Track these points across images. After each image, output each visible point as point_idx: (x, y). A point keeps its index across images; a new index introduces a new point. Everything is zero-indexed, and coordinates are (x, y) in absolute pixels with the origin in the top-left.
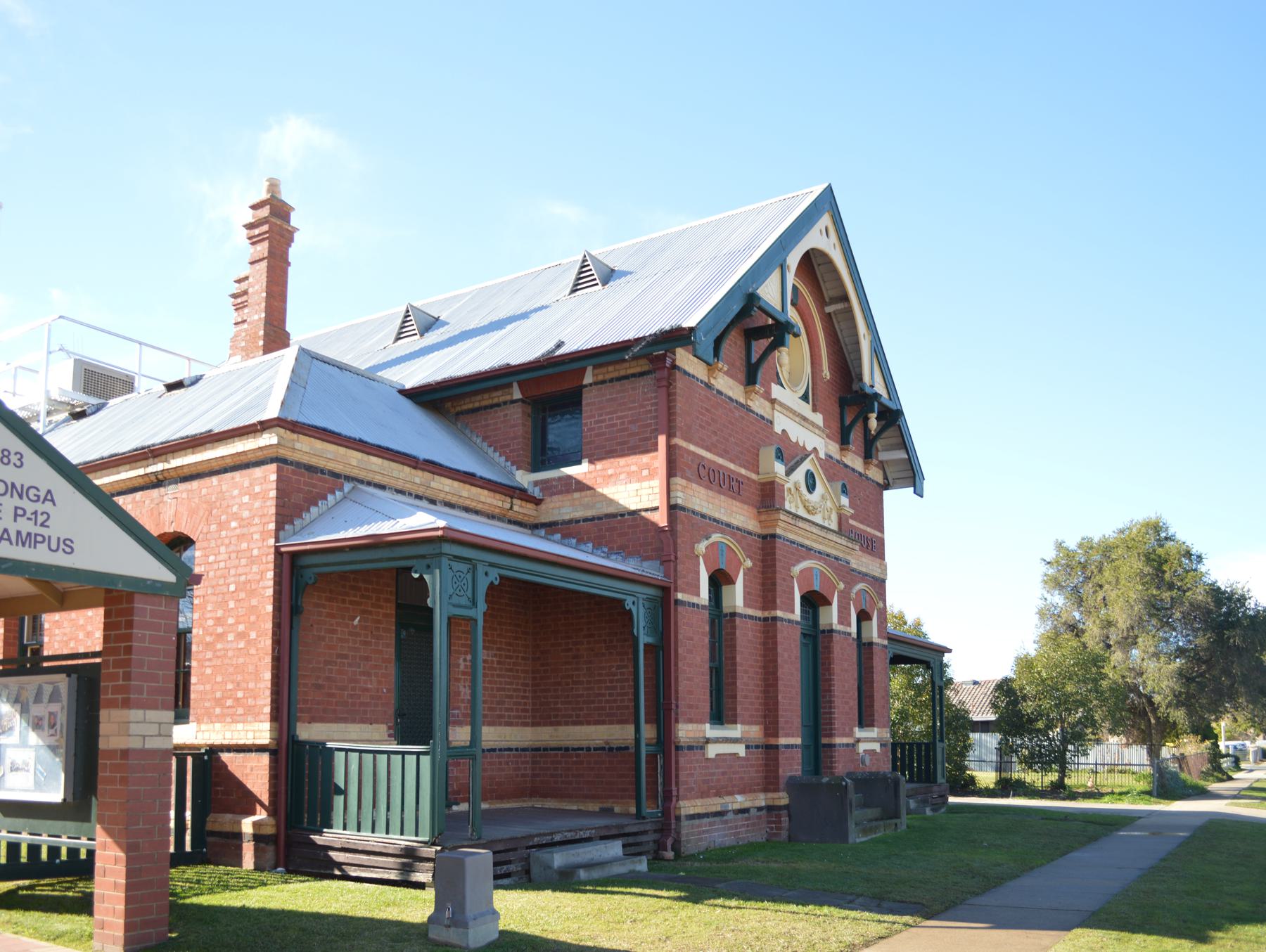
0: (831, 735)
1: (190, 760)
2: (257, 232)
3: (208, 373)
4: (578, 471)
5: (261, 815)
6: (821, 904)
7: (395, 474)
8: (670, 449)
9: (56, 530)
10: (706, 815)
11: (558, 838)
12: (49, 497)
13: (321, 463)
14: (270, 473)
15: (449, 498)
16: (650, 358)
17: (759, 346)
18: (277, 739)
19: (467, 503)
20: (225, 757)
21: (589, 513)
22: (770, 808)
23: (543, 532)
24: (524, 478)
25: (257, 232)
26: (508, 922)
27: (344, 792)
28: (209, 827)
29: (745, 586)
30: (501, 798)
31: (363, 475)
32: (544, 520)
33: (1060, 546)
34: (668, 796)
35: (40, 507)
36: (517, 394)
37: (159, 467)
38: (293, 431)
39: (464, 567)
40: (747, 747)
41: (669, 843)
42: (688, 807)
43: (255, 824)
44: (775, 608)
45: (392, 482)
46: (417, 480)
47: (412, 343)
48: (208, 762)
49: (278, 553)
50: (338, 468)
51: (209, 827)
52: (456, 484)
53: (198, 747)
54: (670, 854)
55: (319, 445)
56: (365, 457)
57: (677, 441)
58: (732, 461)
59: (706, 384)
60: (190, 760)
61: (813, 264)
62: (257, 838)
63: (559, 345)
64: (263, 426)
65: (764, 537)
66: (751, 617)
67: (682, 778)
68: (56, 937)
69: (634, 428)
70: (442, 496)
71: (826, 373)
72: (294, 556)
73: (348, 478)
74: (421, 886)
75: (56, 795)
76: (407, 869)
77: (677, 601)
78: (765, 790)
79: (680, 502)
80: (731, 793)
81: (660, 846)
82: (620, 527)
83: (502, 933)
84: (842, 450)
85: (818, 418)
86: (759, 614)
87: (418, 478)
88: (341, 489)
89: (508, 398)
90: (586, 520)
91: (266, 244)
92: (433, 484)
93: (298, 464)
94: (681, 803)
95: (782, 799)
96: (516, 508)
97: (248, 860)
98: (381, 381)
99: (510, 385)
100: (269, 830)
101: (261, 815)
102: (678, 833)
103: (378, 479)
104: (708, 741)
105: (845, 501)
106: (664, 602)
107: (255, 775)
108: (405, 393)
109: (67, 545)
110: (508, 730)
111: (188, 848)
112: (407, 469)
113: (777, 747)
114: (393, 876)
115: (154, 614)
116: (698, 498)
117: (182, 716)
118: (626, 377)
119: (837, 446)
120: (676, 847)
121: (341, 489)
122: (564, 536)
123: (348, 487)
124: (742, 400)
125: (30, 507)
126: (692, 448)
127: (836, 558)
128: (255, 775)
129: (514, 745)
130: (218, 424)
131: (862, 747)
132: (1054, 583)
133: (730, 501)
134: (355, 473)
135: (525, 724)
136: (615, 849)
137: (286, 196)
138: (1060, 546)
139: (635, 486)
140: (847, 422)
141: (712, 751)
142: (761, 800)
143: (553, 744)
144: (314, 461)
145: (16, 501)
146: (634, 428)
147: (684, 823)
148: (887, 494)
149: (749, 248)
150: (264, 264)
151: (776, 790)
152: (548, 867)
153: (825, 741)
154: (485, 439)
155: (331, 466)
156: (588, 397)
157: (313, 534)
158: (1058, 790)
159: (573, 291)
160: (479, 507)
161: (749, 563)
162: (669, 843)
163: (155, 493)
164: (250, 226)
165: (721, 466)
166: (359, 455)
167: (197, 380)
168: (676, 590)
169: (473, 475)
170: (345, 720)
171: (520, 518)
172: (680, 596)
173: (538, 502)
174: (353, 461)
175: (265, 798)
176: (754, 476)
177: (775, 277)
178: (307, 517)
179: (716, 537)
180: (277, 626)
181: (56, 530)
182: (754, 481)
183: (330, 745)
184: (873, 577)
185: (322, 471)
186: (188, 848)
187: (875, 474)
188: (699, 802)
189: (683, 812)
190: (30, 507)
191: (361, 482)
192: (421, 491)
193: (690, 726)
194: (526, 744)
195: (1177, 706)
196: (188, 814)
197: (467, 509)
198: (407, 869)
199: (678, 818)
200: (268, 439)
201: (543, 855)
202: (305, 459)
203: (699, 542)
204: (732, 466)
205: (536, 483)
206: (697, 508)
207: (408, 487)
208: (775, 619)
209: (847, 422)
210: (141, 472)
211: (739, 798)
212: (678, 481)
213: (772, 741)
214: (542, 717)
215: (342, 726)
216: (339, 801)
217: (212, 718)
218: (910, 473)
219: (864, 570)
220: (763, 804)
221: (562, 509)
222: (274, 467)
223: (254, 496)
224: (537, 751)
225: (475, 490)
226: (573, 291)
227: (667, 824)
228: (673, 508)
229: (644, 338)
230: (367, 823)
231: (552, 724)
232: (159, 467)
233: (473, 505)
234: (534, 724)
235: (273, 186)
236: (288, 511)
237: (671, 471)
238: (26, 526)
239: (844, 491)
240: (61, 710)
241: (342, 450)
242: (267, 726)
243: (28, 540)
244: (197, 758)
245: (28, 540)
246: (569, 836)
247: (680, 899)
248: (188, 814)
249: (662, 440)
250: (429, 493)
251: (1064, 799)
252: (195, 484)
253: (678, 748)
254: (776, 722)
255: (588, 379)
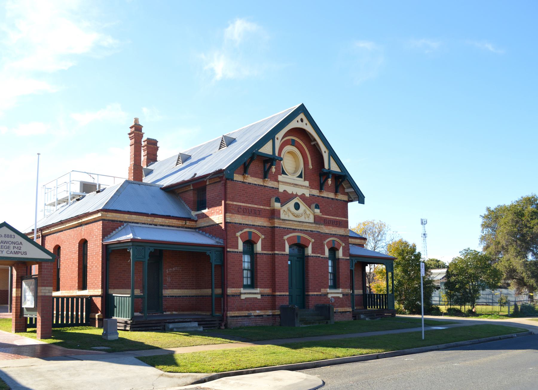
0: (308, 292)
1: (85, 299)
2: (131, 136)
3: (107, 187)
4: (205, 211)
5: (100, 313)
6: (218, 337)
7: (141, 219)
8: (225, 205)
9: (23, 250)
10: (241, 316)
11: (176, 320)
12: (21, 243)
13: (116, 219)
14: (100, 223)
15: (161, 223)
16: (220, 177)
17: (268, 165)
18: (103, 294)
19: (168, 224)
20: (93, 298)
21: (208, 224)
22: (273, 315)
23: (197, 230)
24: (194, 213)
25: (131, 136)
26: (120, 336)
27: (116, 307)
28: (90, 317)
29: (262, 244)
30: (183, 311)
31: (130, 221)
32: (198, 226)
33: (488, 209)
34: (224, 311)
35: (19, 246)
36: (192, 188)
37: (80, 221)
38: (106, 212)
39: (141, 248)
40: (261, 296)
41: (223, 324)
42: (230, 314)
43: (98, 316)
44: (275, 251)
45: (141, 222)
46: (149, 220)
47: (181, 166)
48: (89, 299)
49: (103, 245)
50: (122, 220)
51: (90, 317)
52: (163, 219)
53: (87, 296)
54: (223, 327)
55: (114, 214)
56: (130, 216)
57: (228, 202)
58: (255, 204)
59: (242, 182)
60: (85, 299)
61: (300, 132)
62: (98, 319)
63: (195, 174)
64: (98, 211)
65: (272, 227)
66: (264, 254)
67: (228, 305)
68: (32, 337)
69: (218, 198)
70: (159, 223)
71: (311, 167)
72: (107, 245)
73: (125, 222)
74: (128, 331)
75: (33, 306)
76: (125, 327)
77: (227, 251)
78: (272, 309)
79: (228, 221)
80: (255, 310)
81: (220, 325)
82: (212, 229)
83: (119, 338)
84: (320, 192)
85: (307, 183)
86: (270, 252)
87: (149, 219)
88: (123, 225)
89: (189, 189)
90: (207, 226)
91: (134, 140)
92: (155, 220)
93: (109, 220)
94: (228, 312)
95: (278, 312)
96: (187, 224)
97: (97, 326)
98: (155, 186)
99: (190, 185)
100: (101, 317)
101: (100, 313)
102: (226, 320)
103: (135, 221)
104: (328, 293)
105: (317, 211)
106: (222, 251)
107: (98, 302)
108: (161, 189)
109: (25, 253)
110: (186, 290)
111: (84, 322)
112: (145, 217)
113: (275, 295)
114: (123, 329)
115: (47, 266)
116: (238, 219)
117: (58, 289)
118: (215, 183)
119: (318, 191)
120: (226, 326)
121: (123, 225)
122: (203, 231)
123: (125, 224)
124: (262, 184)
125: (17, 246)
126: (235, 203)
127: (312, 231)
128: (98, 302)
129: (188, 295)
130: (91, 210)
131: (330, 296)
132: (485, 226)
133: (254, 218)
134: (127, 220)
135: (194, 289)
136: (196, 324)
137: (141, 123)
138: (488, 209)
139: (218, 216)
140: (322, 182)
141: (243, 297)
142: (270, 312)
143: (200, 295)
144: (113, 219)
145: (14, 245)
146: (218, 198)
147: (229, 318)
148: (350, 205)
149: (260, 135)
150: (133, 146)
151: (275, 309)
152: (169, 328)
153: (306, 293)
154: (185, 201)
155: (119, 219)
156: (208, 189)
157: (110, 238)
158: (471, 313)
159: (220, 149)
160: (173, 225)
161: (263, 237)
162: (223, 324)
163: (80, 228)
164: (130, 134)
165: (250, 207)
166: (128, 215)
167: (104, 189)
168: (227, 248)
169: (170, 216)
170: (125, 288)
171: (190, 226)
172: (228, 250)
173: (196, 221)
174: (126, 217)
175: (100, 309)
176: (268, 208)
177: (270, 143)
178: (112, 234)
179: (245, 230)
180: (102, 264)
181: (23, 250)
182: (268, 210)
183: (114, 295)
184: (340, 235)
185: (117, 221)
186: (84, 322)
187: (341, 197)
188: (236, 312)
189: (228, 315)
190: (17, 246)
191: (130, 222)
192: (151, 223)
193: (231, 289)
194: (193, 295)
195: (532, 277)
196: (84, 314)
197: (169, 226)
198: (125, 327)
199: (227, 317)
200: (99, 215)
201: (167, 324)
202: (111, 219)
203: (238, 232)
204: (256, 206)
205: (196, 215)
206: (237, 222)
207: (146, 222)
208: (275, 254)
209: (322, 182)
210: (77, 222)
211: (258, 312)
212: (228, 214)
213: (274, 294)
214: (198, 287)
215: (124, 290)
216: (115, 309)
217: (91, 288)
218: (357, 196)
219: (334, 233)
220: (271, 314)
221: (202, 223)
222: (101, 222)
223: (98, 229)
224: (197, 296)
225: (171, 220)
226: (220, 149)
227: (223, 319)
228: (226, 223)
229: (209, 174)
230: (120, 315)
231: (171, 289)
232: (80, 221)
233: (171, 224)
234: (196, 289)
235: (136, 120)
236: (106, 233)
237: (226, 212)
238: (16, 250)
239: (317, 207)
240: (33, 287)
241: (122, 215)
242: (100, 290)
243: (17, 253)
244: (87, 299)
245: (17, 253)
246: (181, 320)
247: (187, 335)
248: (84, 314)
249: (223, 202)
250: (154, 223)
251: (463, 317)
252: (88, 226)
253: (227, 296)
254: (275, 288)
255: (208, 183)
